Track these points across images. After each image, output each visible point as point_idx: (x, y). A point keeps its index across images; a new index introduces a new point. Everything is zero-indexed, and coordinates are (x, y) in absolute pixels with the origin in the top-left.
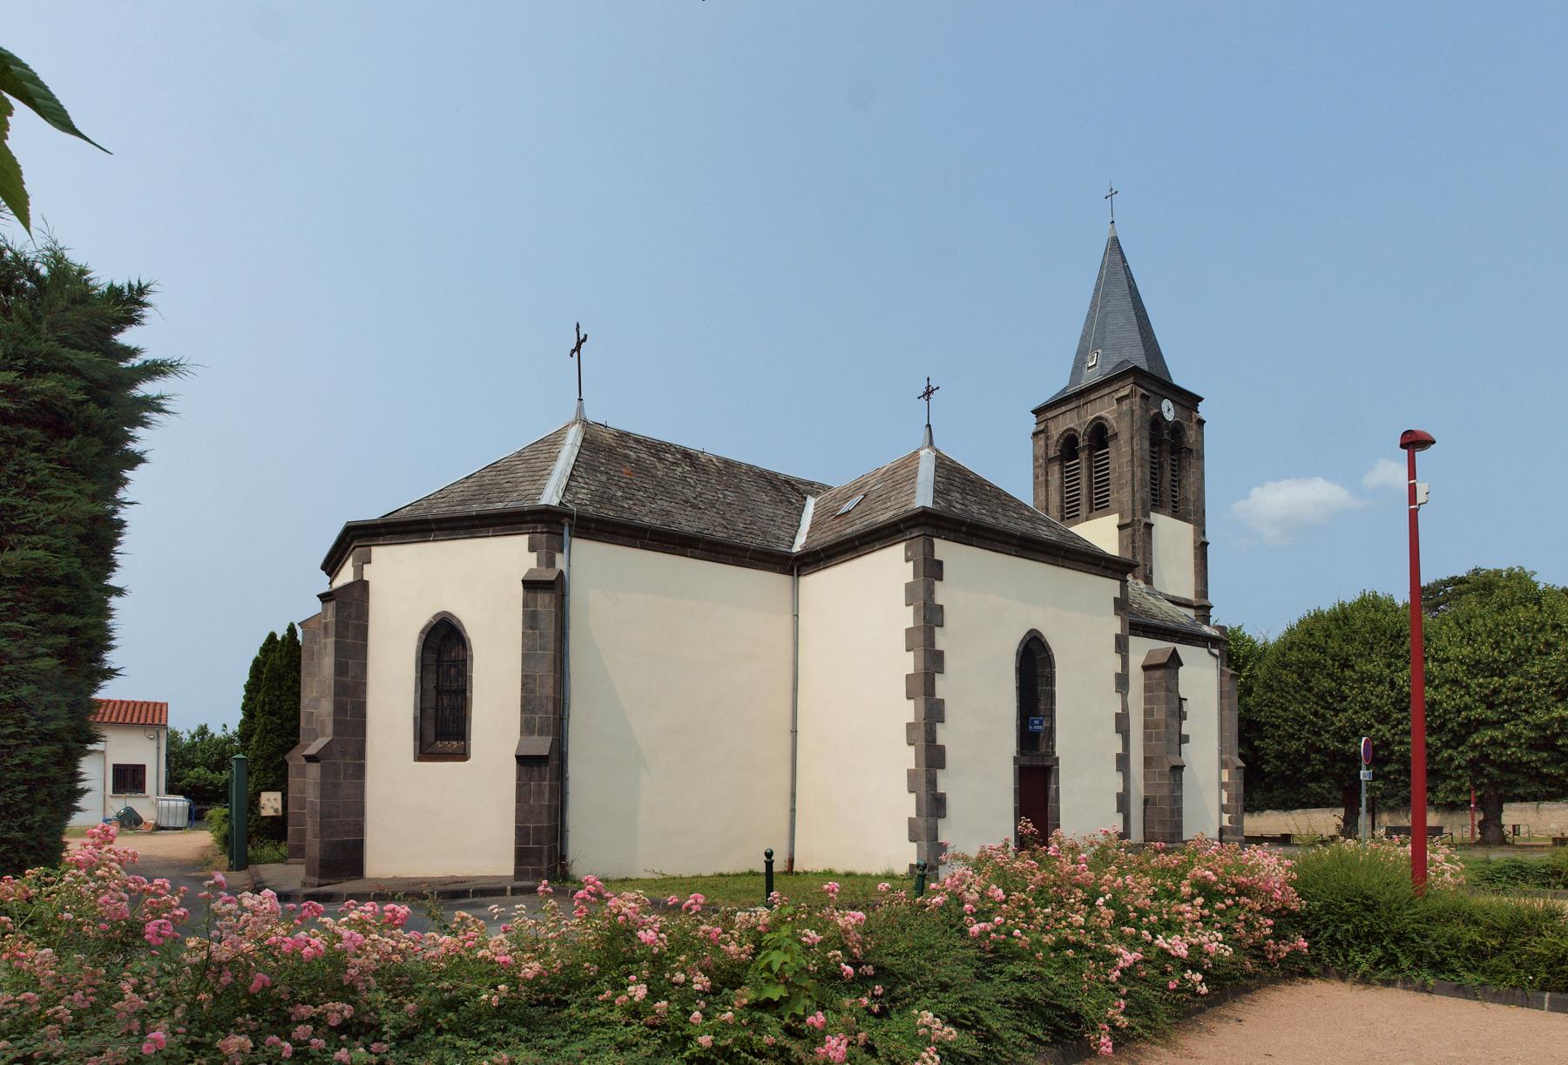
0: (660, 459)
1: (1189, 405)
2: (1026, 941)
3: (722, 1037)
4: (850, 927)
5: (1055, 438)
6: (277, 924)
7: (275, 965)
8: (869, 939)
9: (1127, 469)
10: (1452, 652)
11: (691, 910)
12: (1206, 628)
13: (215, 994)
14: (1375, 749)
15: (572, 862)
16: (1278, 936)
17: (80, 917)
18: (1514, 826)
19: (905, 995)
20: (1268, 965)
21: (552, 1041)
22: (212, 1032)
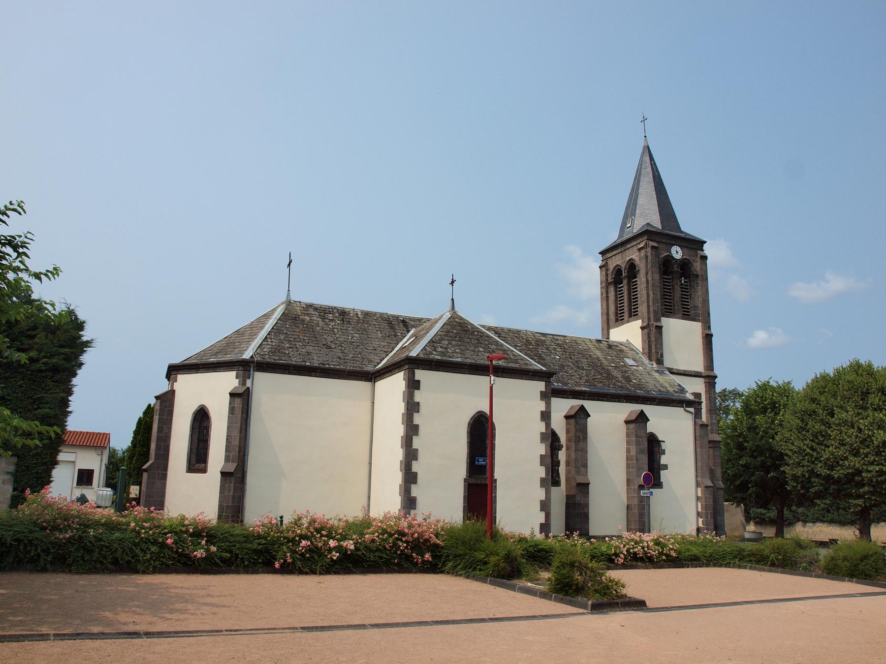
5: (612, 270)
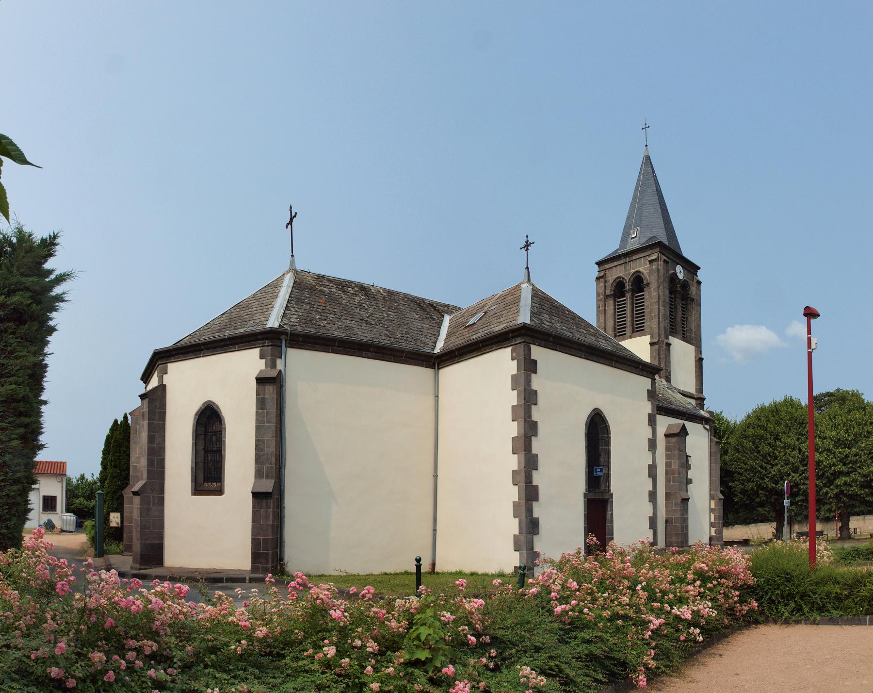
0: (344, 292)
1: (692, 271)
2: (592, 616)
3: (386, 685)
4: (473, 610)
5: (611, 282)
6: (118, 590)
7: (117, 614)
8: (487, 618)
9: (655, 307)
10: (828, 433)
11: (366, 597)
12: (702, 412)
13: (88, 626)
14: (792, 487)
15: (287, 563)
16: (742, 601)
17: (29, 576)
18: (854, 529)
19: (512, 656)
20: (737, 619)
21: (275, 680)
22: (87, 648)
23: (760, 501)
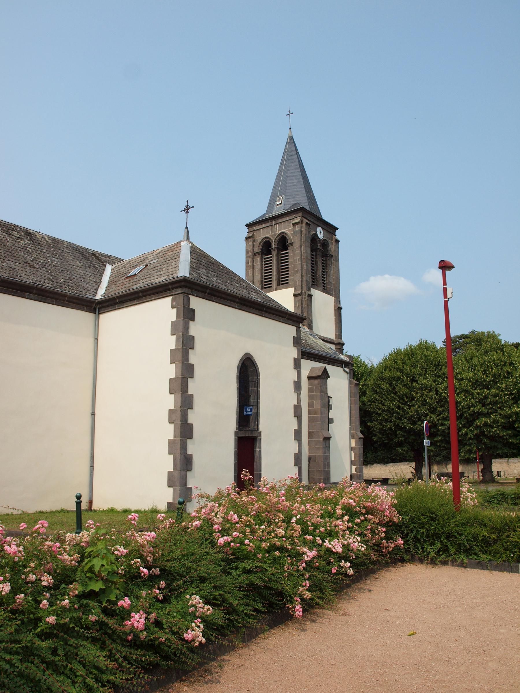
1: (331, 231)
2: (252, 547)
4: (146, 543)
5: (259, 241)
9: (298, 263)
10: (465, 375)
12: (342, 356)
16: (388, 538)
18: (498, 472)
19: (179, 587)
23: (398, 442)
